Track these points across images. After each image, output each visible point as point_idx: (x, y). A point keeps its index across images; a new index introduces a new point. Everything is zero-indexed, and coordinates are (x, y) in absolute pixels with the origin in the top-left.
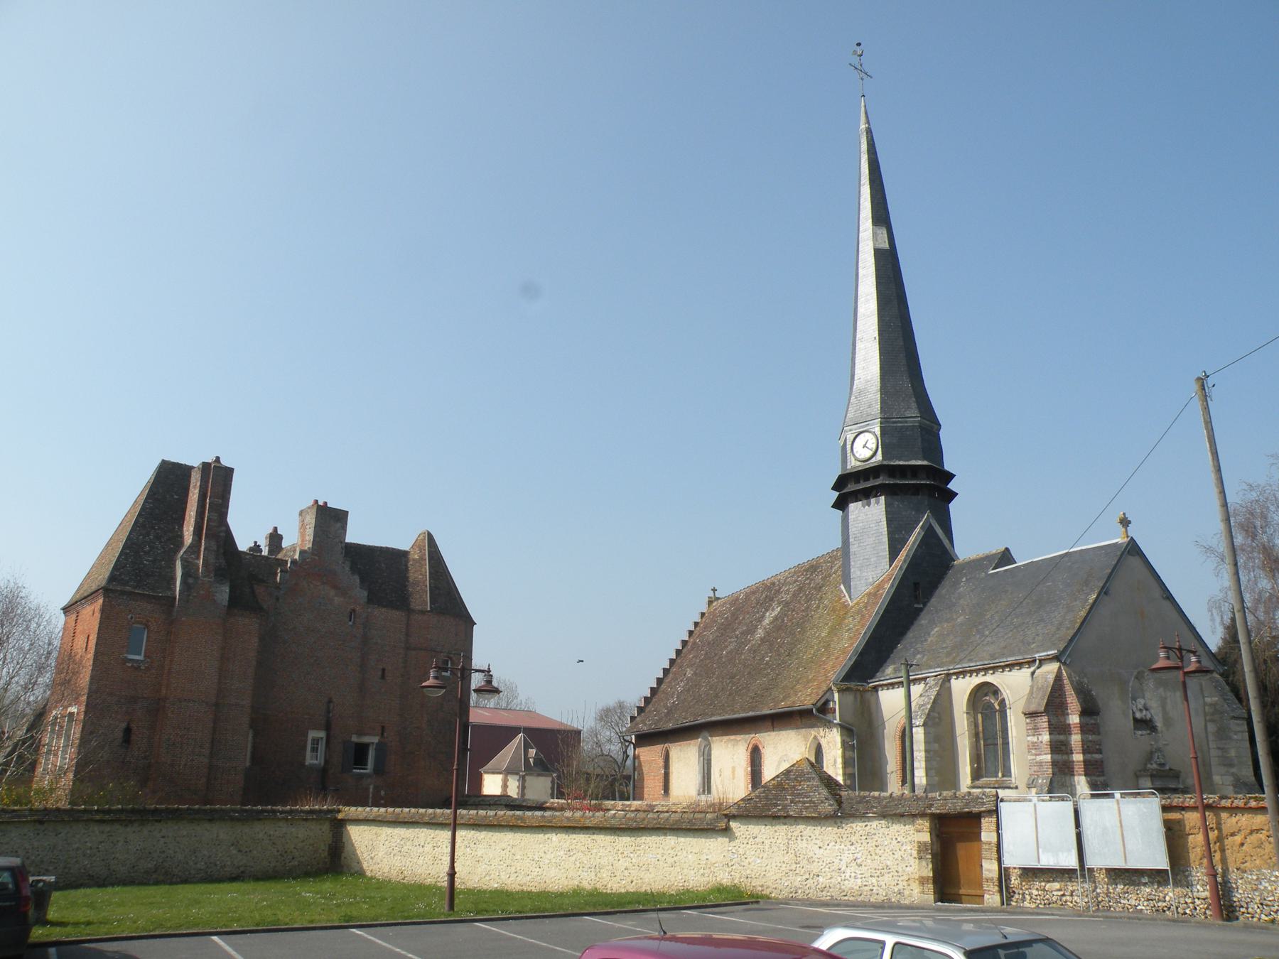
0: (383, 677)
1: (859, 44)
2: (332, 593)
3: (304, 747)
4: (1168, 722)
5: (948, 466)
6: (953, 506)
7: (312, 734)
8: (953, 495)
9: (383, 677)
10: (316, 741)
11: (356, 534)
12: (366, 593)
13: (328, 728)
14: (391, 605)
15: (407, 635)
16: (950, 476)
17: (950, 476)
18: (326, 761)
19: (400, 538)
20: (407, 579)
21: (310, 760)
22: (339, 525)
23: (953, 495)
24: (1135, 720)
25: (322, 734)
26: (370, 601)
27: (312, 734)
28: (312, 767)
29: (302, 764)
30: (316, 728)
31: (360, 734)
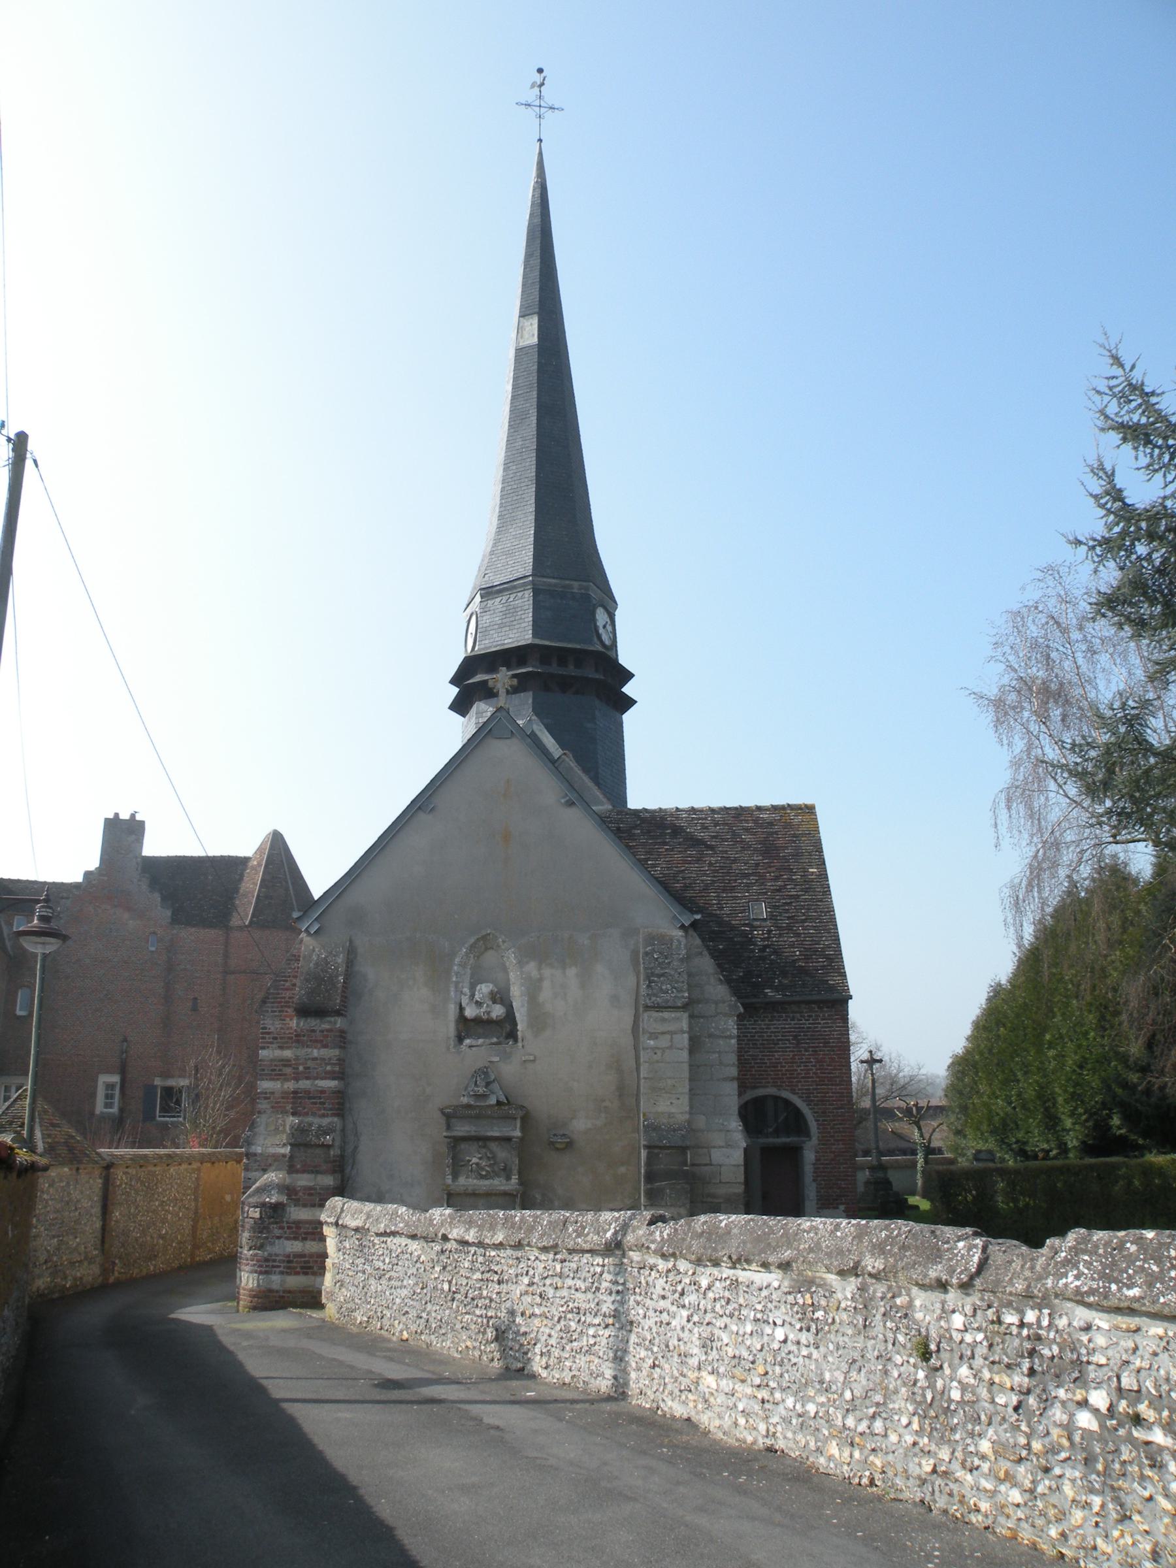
0: (195, 1009)
1: (540, 71)
2: (126, 915)
3: (93, 1095)
4: (540, 1021)
5: (625, 658)
6: (628, 718)
7: (104, 1079)
8: (629, 703)
9: (195, 1009)
10: (110, 1086)
11: (155, 846)
12: (169, 913)
13: (123, 1071)
14: (205, 923)
15: (226, 956)
16: (627, 676)
17: (627, 676)
18: (121, 1110)
19: (240, 841)
20: (237, 890)
21: (100, 1108)
22: (133, 837)
23: (629, 703)
24: (462, 1019)
25: (115, 1079)
26: (175, 920)
27: (104, 1079)
28: (103, 1117)
29: (92, 1113)
30: (108, 1071)
31: (166, 1075)
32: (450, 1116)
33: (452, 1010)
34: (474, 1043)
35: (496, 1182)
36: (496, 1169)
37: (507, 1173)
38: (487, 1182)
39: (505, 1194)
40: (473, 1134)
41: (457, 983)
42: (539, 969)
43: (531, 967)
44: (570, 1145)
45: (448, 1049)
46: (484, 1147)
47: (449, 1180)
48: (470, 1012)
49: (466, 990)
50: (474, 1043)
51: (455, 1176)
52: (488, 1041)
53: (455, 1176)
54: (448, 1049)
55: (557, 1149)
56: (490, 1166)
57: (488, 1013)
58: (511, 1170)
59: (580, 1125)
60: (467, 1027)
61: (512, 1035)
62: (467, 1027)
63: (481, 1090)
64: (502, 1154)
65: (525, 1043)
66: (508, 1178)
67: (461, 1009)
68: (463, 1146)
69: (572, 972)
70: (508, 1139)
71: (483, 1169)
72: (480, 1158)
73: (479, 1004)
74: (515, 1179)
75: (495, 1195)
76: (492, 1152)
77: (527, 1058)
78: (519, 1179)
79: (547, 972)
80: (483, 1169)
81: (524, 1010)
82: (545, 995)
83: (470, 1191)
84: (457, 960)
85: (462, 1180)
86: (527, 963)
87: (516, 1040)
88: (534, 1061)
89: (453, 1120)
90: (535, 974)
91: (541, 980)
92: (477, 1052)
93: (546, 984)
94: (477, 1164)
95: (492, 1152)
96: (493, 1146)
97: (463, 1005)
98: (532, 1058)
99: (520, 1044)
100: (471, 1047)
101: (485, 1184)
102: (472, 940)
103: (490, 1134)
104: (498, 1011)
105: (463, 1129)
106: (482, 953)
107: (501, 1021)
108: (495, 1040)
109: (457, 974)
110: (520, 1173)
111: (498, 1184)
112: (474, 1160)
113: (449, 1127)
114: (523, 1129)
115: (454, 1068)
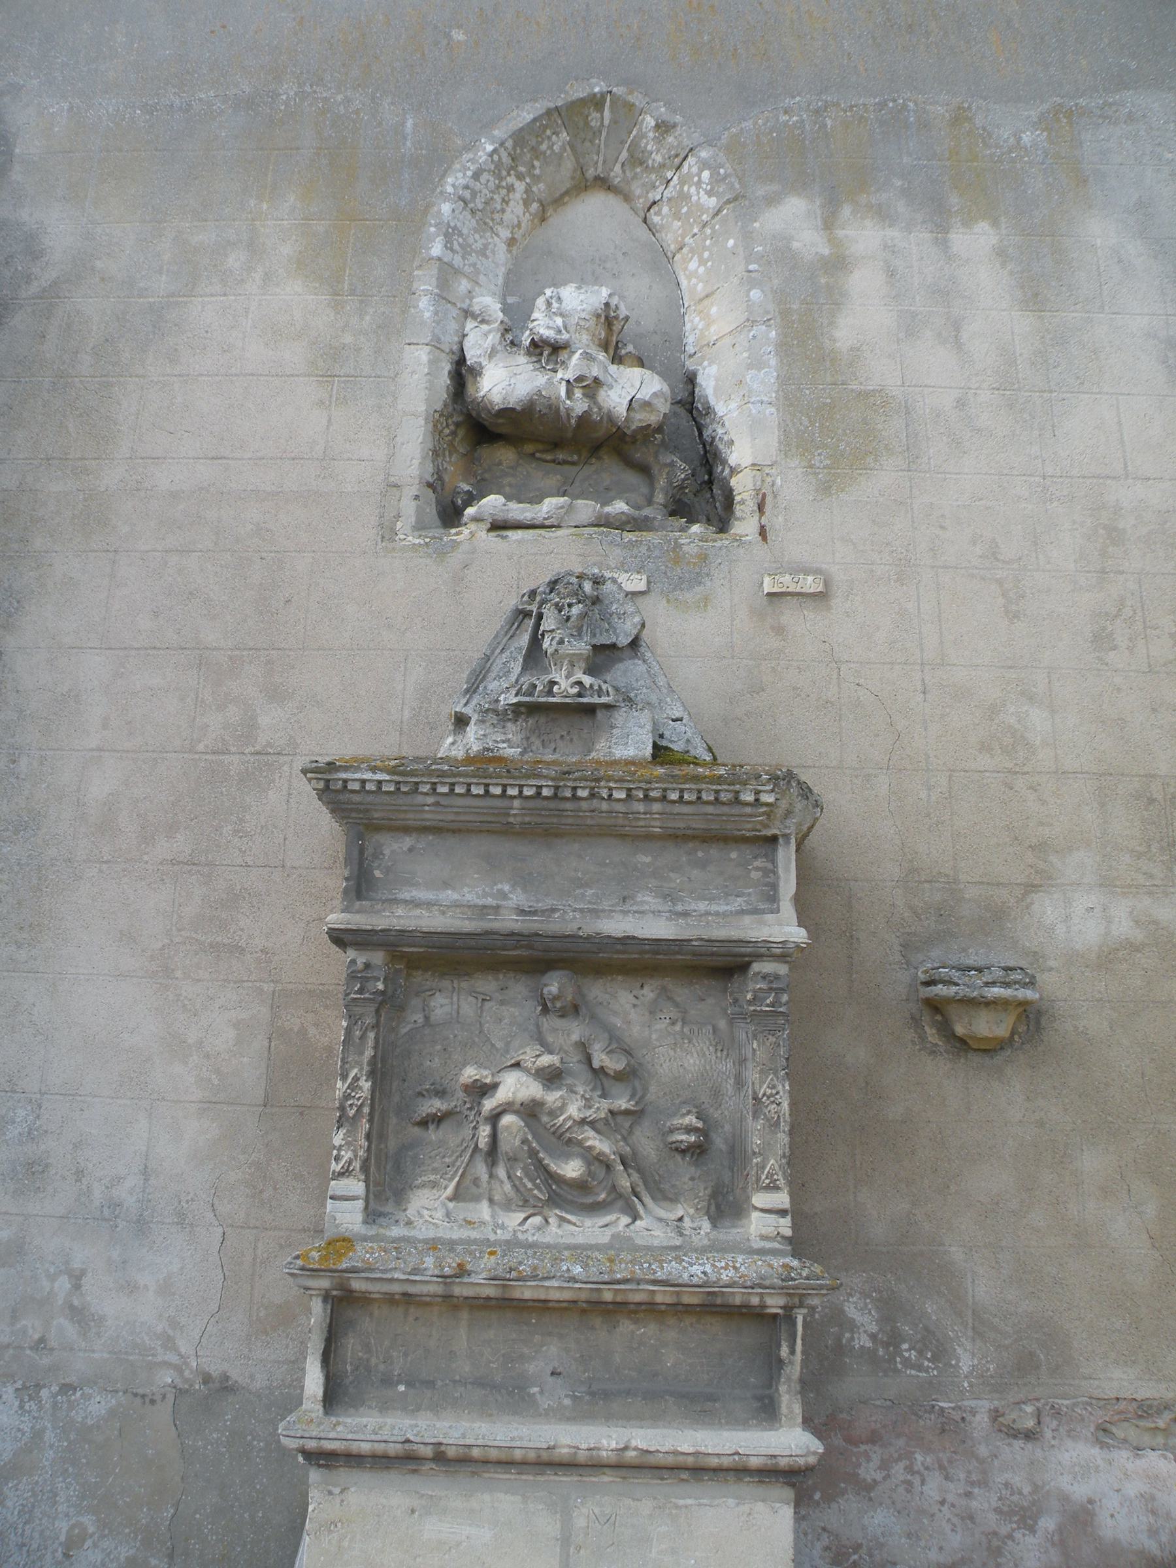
4: (837, 423)
32: (371, 811)
33: (419, 385)
34: (518, 511)
35: (652, 1227)
36: (646, 1144)
37: (712, 1169)
38: (590, 1230)
39: (715, 1308)
40: (509, 922)
41: (447, 273)
42: (829, 224)
43: (793, 218)
44: (1031, 1019)
45: (388, 533)
46: (574, 1010)
47: (348, 1216)
48: (503, 382)
49: (489, 302)
50: (518, 511)
51: (388, 1183)
52: (586, 509)
53: (388, 1183)
54: (388, 533)
55: (963, 1045)
56: (611, 1123)
57: (592, 387)
58: (737, 1154)
59: (1075, 923)
60: (483, 439)
61: (704, 493)
62: (483, 439)
63: (565, 682)
64: (678, 1048)
65: (775, 519)
66: (725, 1206)
67: (462, 374)
68: (446, 1003)
69: (976, 241)
70: (724, 966)
71: (565, 1143)
72: (551, 1077)
73: (547, 351)
74: (765, 1218)
75: (649, 1310)
76: (618, 1045)
77: (787, 582)
78: (797, 1213)
79: (864, 237)
80: (565, 1143)
81: (764, 381)
82: (864, 318)
83: (479, 1283)
84: (454, 181)
85: (429, 1211)
86: (772, 201)
87: (721, 515)
88: (821, 597)
89: (393, 846)
90: (809, 241)
91: (838, 263)
92: (548, 536)
93: (864, 283)
94: (531, 1111)
95: (618, 1045)
96: (626, 1006)
97: (471, 356)
98: (810, 584)
99: (745, 526)
100: (499, 526)
101: (577, 1245)
102: (526, 115)
103: (617, 925)
104: (631, 390)
105: (443, 895)
106: (559, 201)
107: (646, 434)
108: (619, 507)
109: (450, 234)
110: (801, 1172)
111: (664, 1241)
112: (514, 1087)
113: (361, 885)
114: (805, 912)
115: (408, 634)
